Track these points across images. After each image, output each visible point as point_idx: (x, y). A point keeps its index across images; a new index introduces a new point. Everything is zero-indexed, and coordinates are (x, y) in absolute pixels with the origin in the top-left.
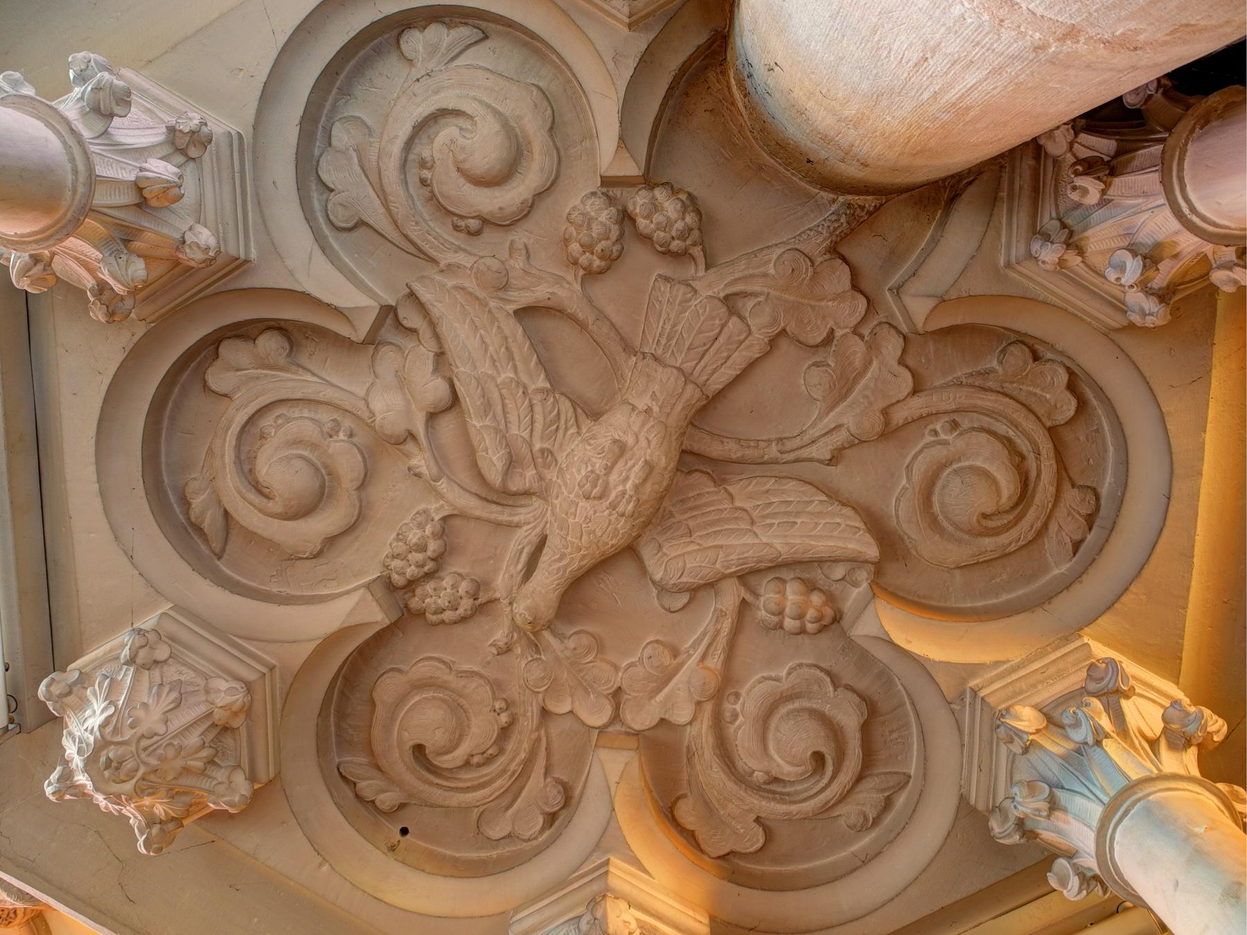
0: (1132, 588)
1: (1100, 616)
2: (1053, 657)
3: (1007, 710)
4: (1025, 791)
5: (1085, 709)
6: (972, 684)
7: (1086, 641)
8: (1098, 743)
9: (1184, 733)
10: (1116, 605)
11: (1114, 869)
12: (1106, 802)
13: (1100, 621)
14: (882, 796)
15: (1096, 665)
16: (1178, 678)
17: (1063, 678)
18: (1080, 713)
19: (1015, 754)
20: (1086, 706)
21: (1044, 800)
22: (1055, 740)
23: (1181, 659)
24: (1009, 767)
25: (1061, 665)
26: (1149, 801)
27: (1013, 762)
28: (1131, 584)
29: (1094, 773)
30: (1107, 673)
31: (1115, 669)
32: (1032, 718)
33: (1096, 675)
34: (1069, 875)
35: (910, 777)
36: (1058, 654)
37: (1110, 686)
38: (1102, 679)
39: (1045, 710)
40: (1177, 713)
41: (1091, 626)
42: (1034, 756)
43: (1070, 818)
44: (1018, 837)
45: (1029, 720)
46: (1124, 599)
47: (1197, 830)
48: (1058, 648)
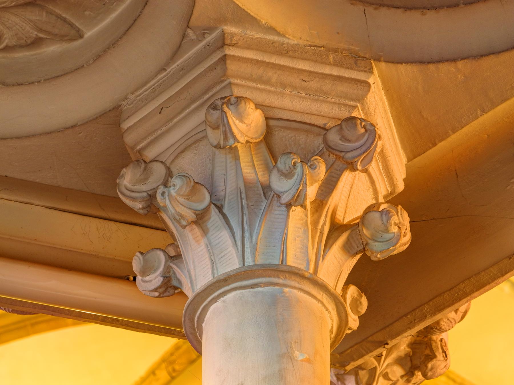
0: (460, 64)
1: (407, 62)
2: (327, 70)
3: (239, 99)
4: (185, 190)
5: (307, 170)
6: (229, 29)
7: (371, 81)
8: (289, 206)
9: (367, 244)
10: (430, 66)
11: (200, 314)
12: (246, 264)
13: (402, 68)
14: (34, 33)
15: (356, 124)
16: (415, 157)
17: (317, 100)
18: (299, 169)
19: (206, 137)
20: (310, 167)
21: (195, 211)
22: (255, 160)
23: (434, 145)
24: (190, 142)
25: (327, 86)
26: (283, 292)
27: (198, 141)
28: (462, 59)
29: (260, 226)
30: (357, 141)
31: (368, 145)
32: (253, 125)
33: (348, 133)
34: (156, 270)
35: (81, 36)
36: (335, 71)
37: (349, 155)
38: (349, 141)
39: (272, 123)
40: (380, 223)
41: (390, 65)
42: (221, 157)
43: (203, 242)
44: (141, 206)
45: (248, 125)
46: (444, 67)
47: (297, 353)
48: (338, 64)
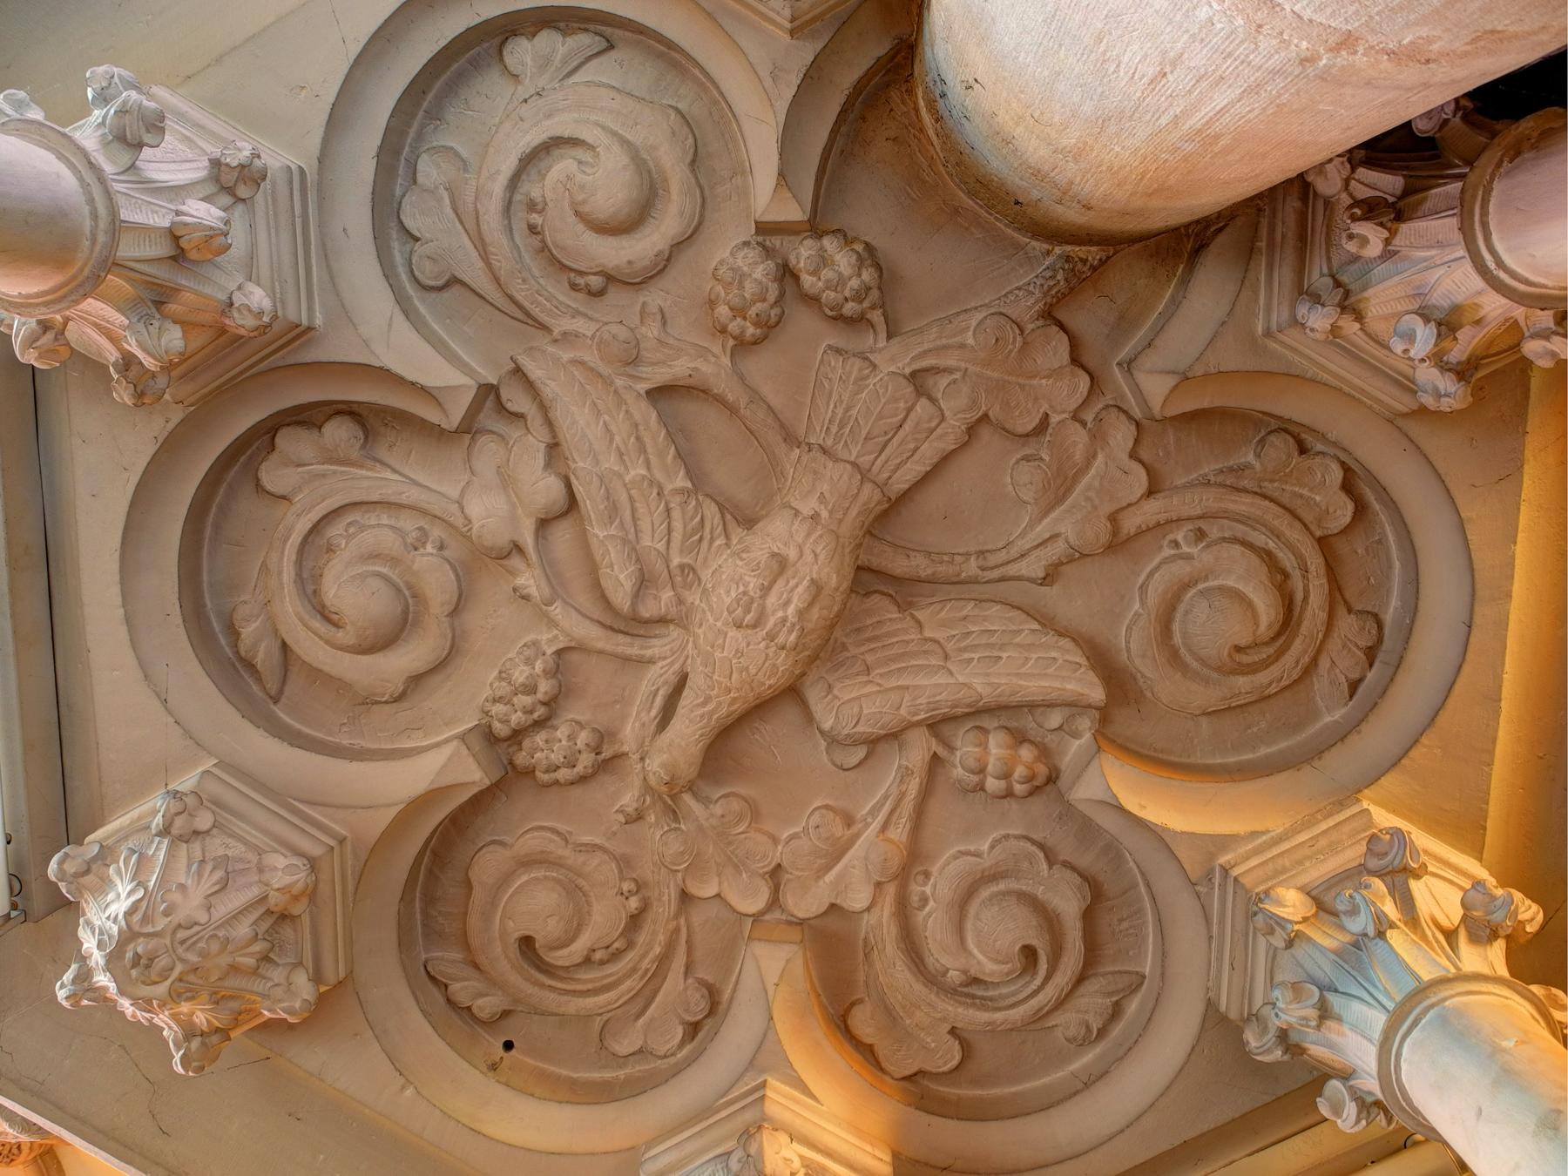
0: (1424, 740)
1: (1383, 775)
2: (1324, 826)
3: (1267, 892)
4: (1289, 995)
5: (1364, 892)
6: (1222, 860)
7: (1365, 806)
8: (1381, 935)
9: (1488, 922)
10: (1403, 761)
11: (1401, 1094)
12: (1391, 1009)
13: (1383, 781)
14: (1108, 1001)
15: (1378, 837)
16: (1482, 853)
17: (1337, 852)
18: (1358, 897)
19: (1276, 949)
20: (1365, 887)
21: (1313, 1006)
22: (1327, 930)
23: (1485, 829)
24: (1269, 965)
25: (1334, 836)
26: (1444, 1008)
27: (1274, 958)
28: (1422, 735)
29: (1375, 973)
30: (1392, 847)
31: (1402, 842)
32: (1297, 903)
33: (1379, 848)
34: (1344, 1101)
35: (1144, 977)
36: (1331, 822)
37: (1396, 862)
38: (1386, 854)
39: (1313, 893)
40: (1480, 897)
41: (1372, 787)
42: (1300, 950)
43: (1345, 1029)
44: (1280, 1053)
45: (1294, 906)
46: (1414, 753)
47: (1505, 1044)
48: (1330, 815)
